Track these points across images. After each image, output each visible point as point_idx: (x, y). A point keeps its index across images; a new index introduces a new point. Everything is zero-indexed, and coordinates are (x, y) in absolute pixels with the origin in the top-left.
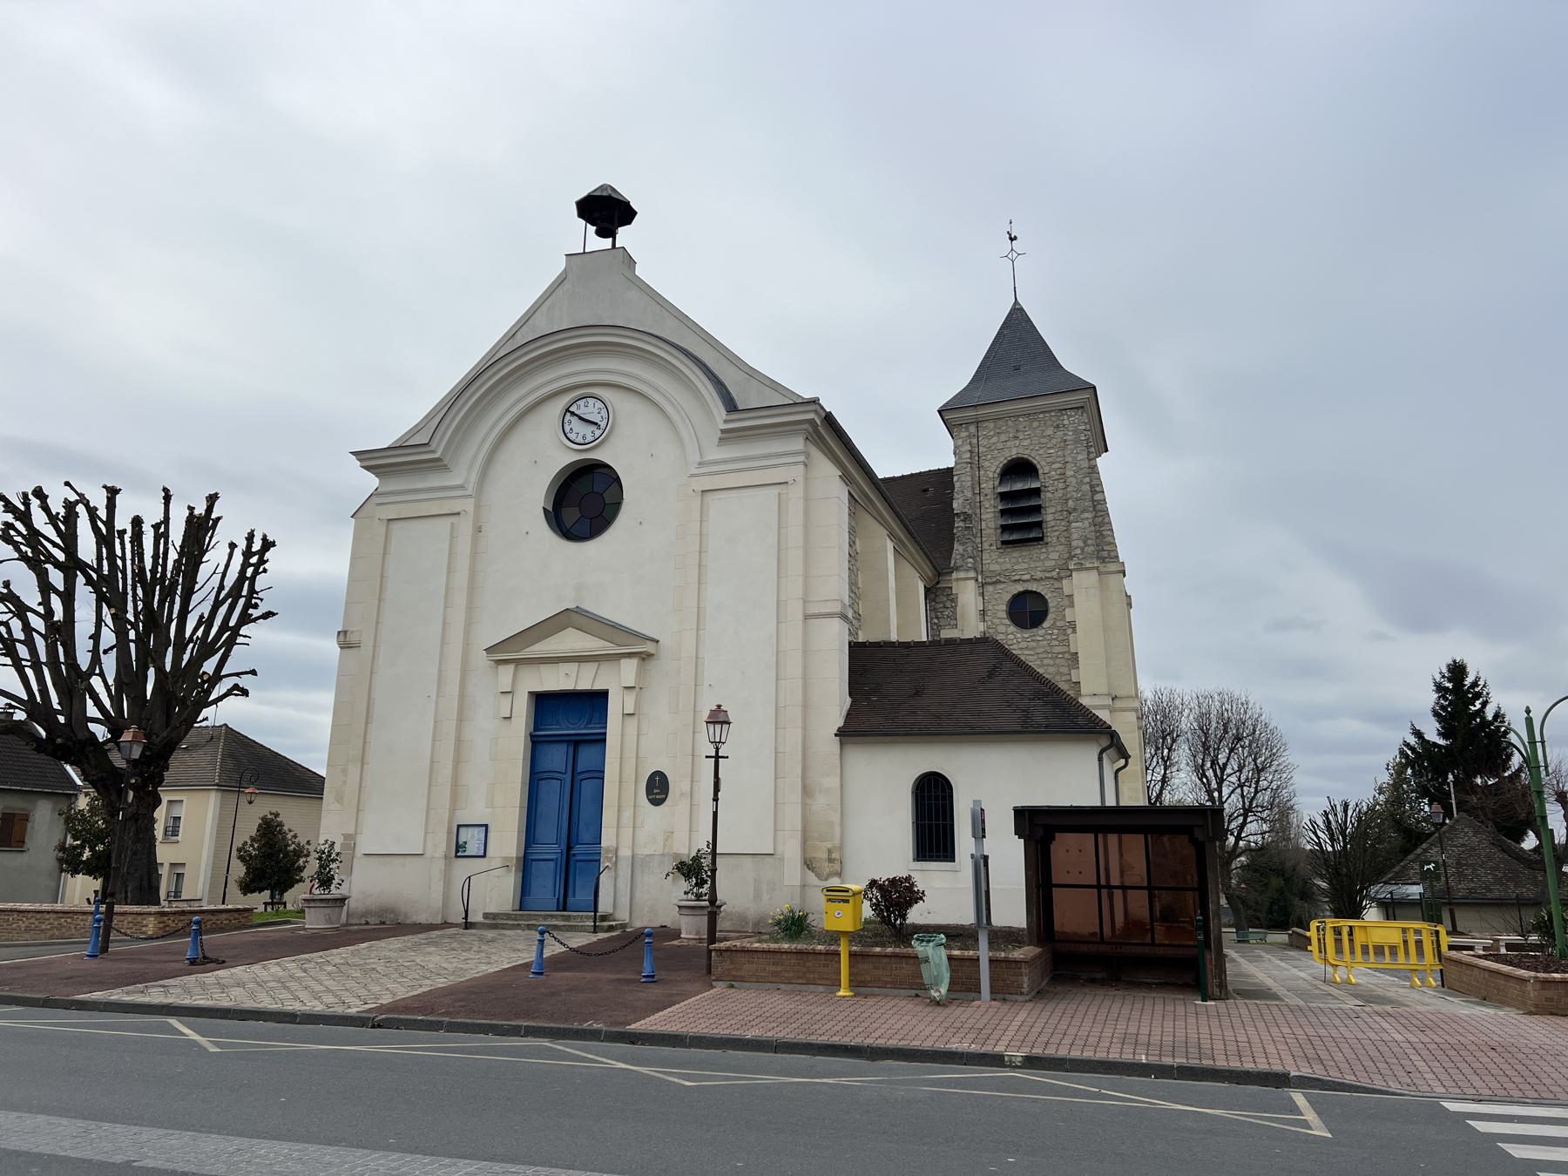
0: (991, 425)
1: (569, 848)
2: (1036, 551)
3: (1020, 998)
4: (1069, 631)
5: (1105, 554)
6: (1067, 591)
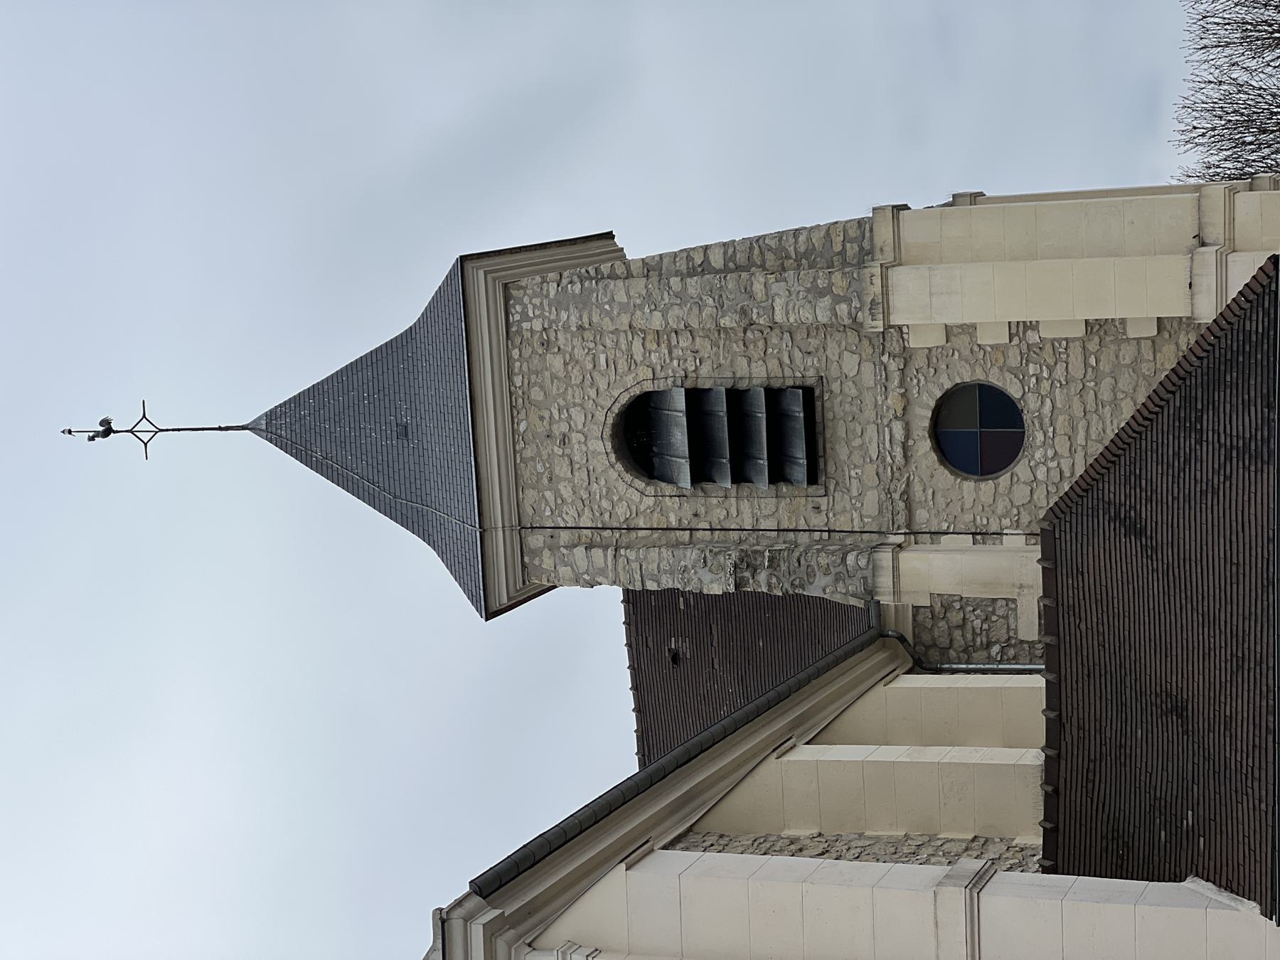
0: (530, 496)
2: (836, 407)
4: (1032, 337)
5: (852, 249)
6: (937, 339)
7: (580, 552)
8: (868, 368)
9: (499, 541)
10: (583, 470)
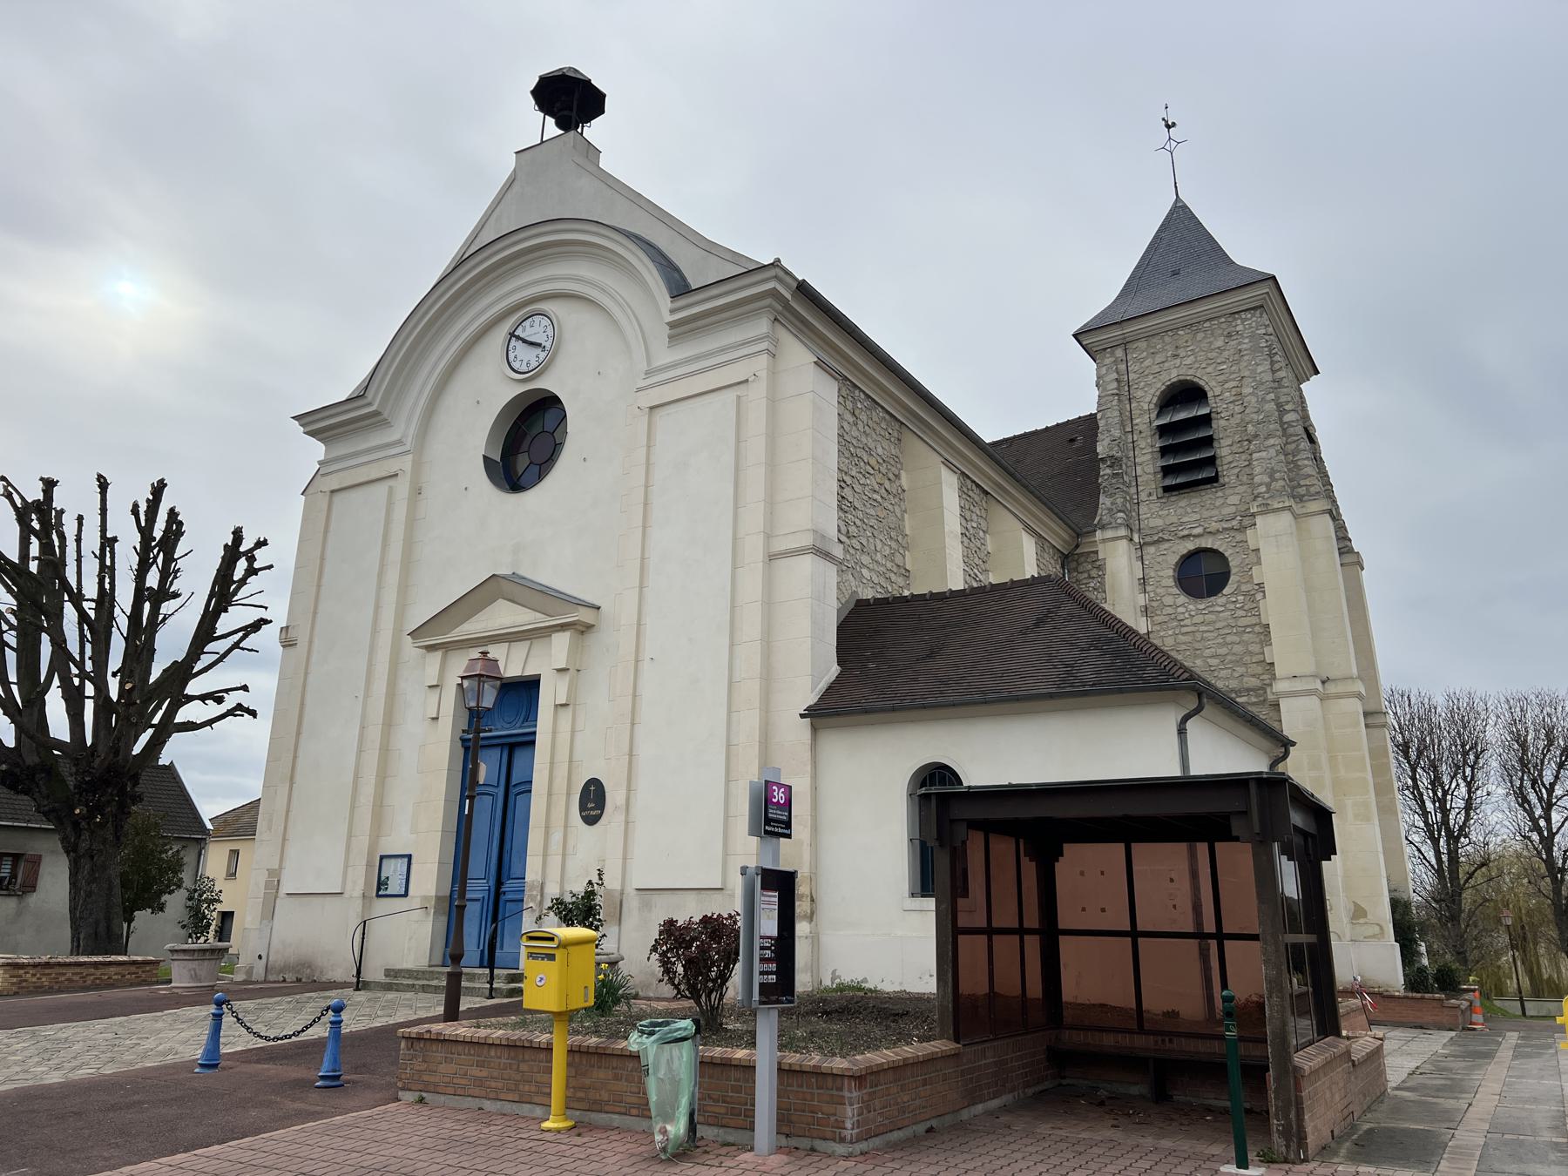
0: (1143, 344)
1: (499, 883)
2: (1208, 496)
3: (840, 1149)
4: (1259, 596)
5: (1302, 491)
6: (1252, 545)
7: (1115, 376)
8: (1233, 509)
9: (1116, 332)
10: (1158, 371)
